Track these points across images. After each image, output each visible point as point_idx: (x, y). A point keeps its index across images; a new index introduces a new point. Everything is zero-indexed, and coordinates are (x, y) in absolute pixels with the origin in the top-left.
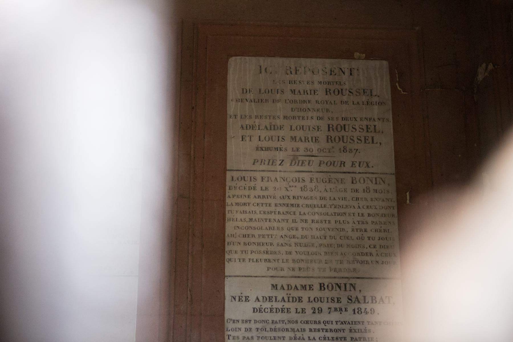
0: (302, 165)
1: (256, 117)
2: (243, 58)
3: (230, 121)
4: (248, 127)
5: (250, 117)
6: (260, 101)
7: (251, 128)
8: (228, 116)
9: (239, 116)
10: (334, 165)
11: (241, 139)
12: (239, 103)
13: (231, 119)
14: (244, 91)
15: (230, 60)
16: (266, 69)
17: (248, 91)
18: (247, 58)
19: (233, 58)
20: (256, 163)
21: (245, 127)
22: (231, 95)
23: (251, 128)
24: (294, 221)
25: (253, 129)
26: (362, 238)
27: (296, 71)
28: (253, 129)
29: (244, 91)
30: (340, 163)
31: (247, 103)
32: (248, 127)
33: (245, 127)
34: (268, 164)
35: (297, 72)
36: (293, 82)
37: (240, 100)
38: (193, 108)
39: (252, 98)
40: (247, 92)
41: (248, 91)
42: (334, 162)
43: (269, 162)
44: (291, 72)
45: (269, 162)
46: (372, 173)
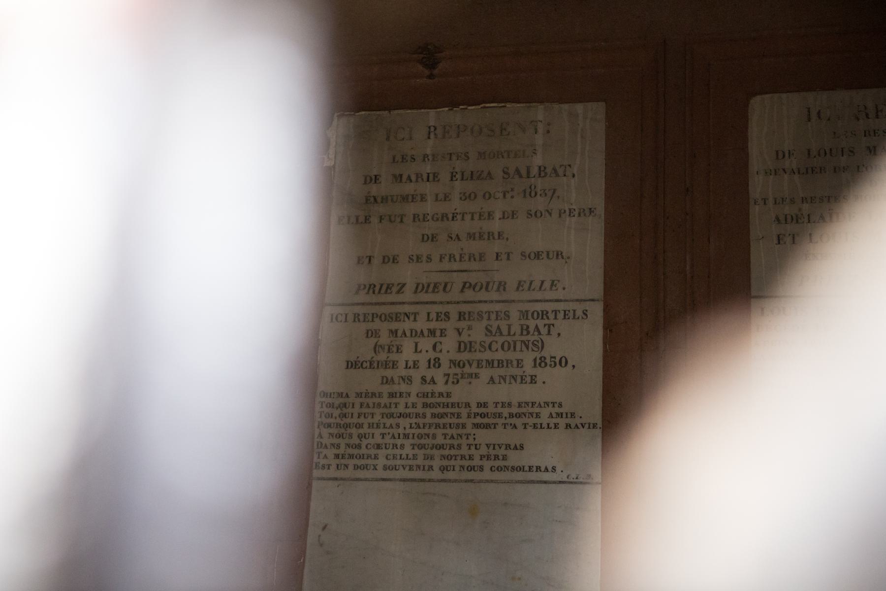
0: (386, 292)
1: (804, 200)
2: (776, 95)
3: (755, 211)
4: (789, 220)
5: (792, 201)
6: (810, 171)
7: (795, 221)
8: (752, 202)
9: (771, 200)
10: (487, 289)
11: (776, 241)
12: (772, 177)
13: (757, 207)
14: (779, 155)
15: (752, 101)
16: (819, 113)
17: (787, 155)
18: (784, 96)
19: (758, 98)
20: (465, 290)
21: (782, 218)
22: (755, 164)
23: (795, 221)
24: (360, 426)
25: (797, 222)
26: (443, 469)
27: (877, 112)
28: (797, 222)
29: (779, 155)
30: (496, 284)
31: (786, 176)
32: (789, 220)
33: (782, 218)
34: (379, 292)
35: (880, 114)
36: (872, 133)
37: (773, 171)
38: (687, 190)
39: (429, 152)
40: (784, 156)
41: (787, 155)
42: (488, 283)
43: (380, 289)
44: (867, 115)
45: (380, 289)
46: (557, 301)
